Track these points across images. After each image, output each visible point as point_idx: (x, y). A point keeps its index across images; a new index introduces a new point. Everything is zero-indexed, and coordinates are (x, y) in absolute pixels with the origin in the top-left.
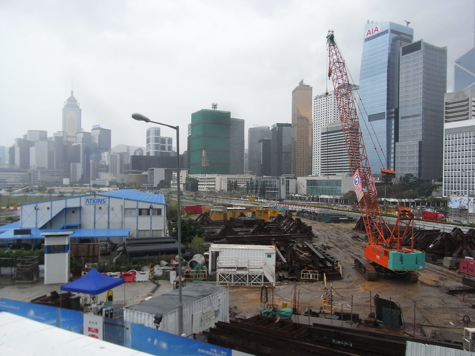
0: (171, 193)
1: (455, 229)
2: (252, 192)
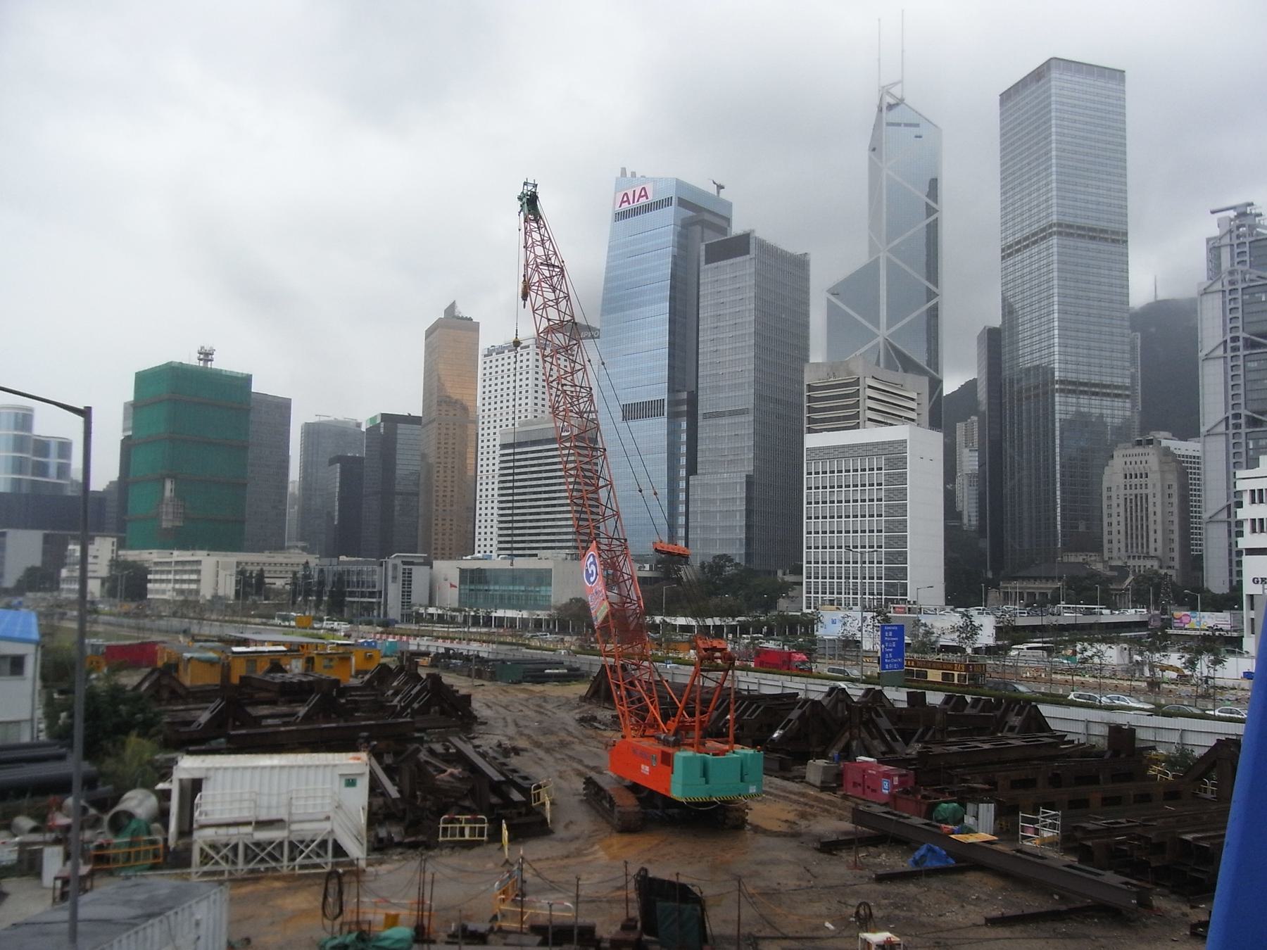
0: (59, 606)
1: (832, 689)
2: (306, 601)
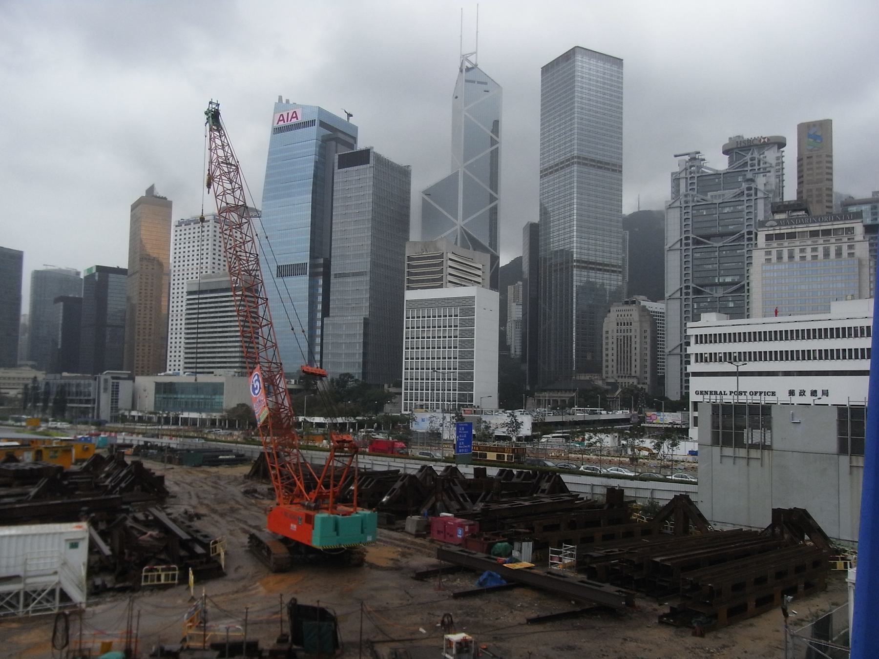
1: (423, 467)
2: (35, 407)
